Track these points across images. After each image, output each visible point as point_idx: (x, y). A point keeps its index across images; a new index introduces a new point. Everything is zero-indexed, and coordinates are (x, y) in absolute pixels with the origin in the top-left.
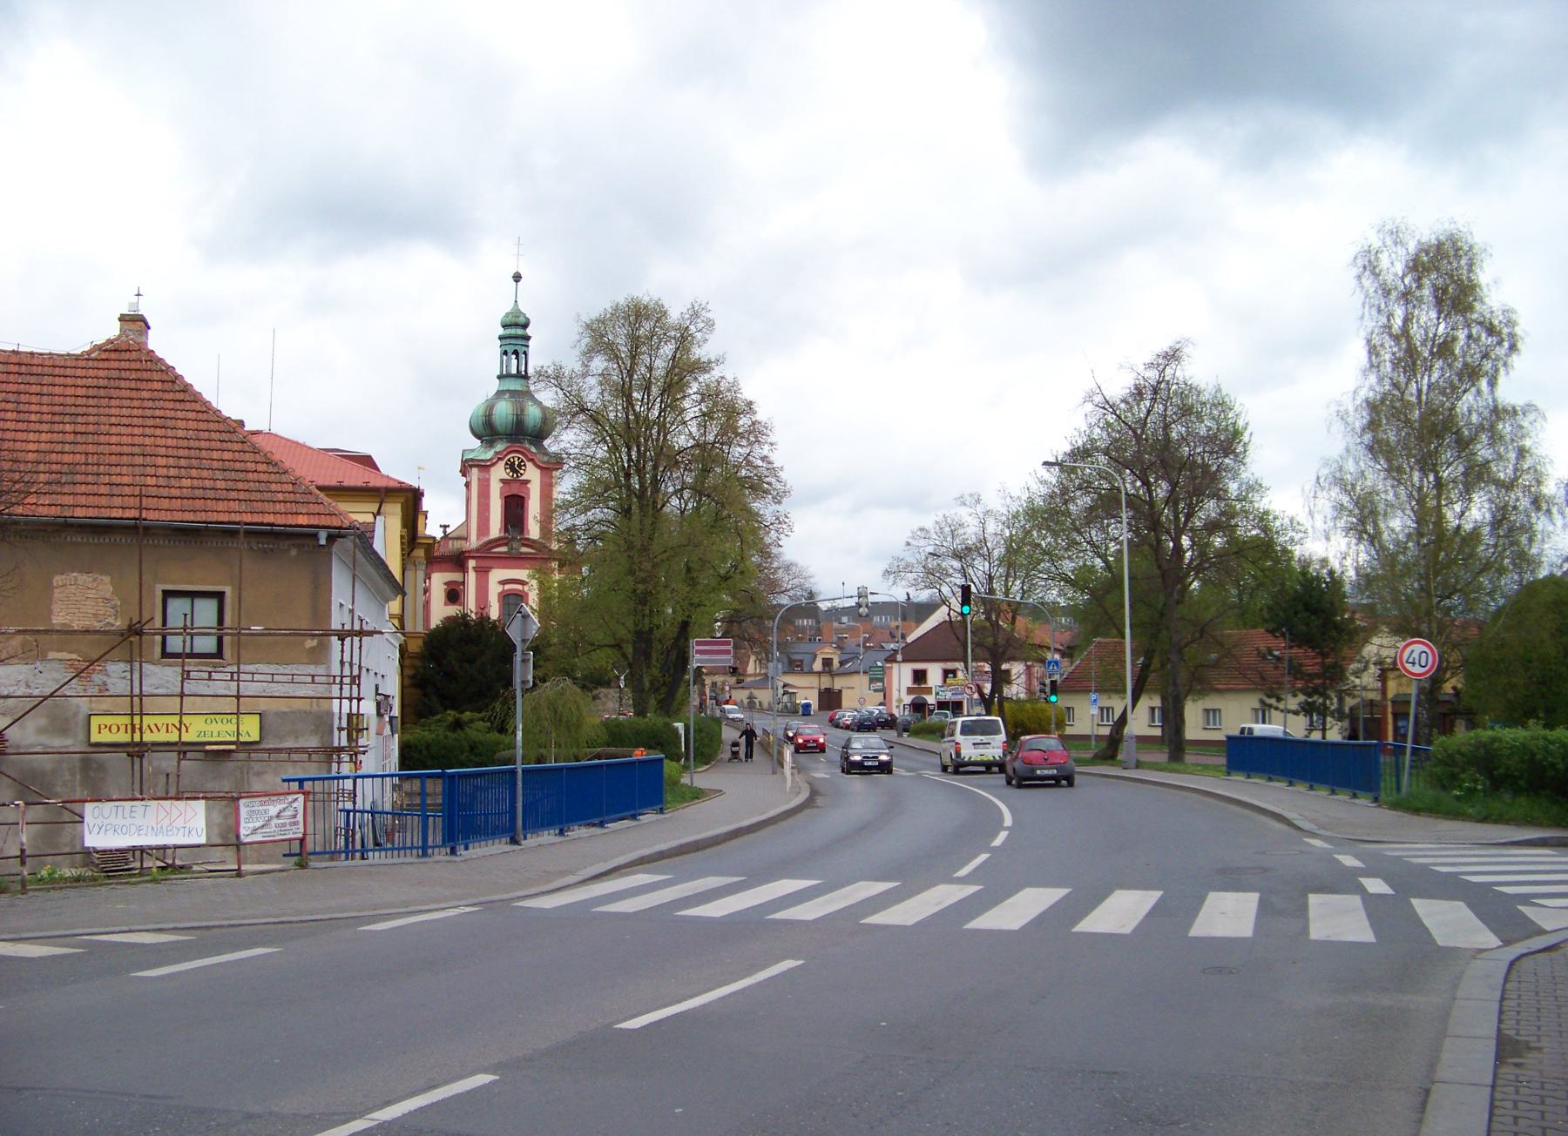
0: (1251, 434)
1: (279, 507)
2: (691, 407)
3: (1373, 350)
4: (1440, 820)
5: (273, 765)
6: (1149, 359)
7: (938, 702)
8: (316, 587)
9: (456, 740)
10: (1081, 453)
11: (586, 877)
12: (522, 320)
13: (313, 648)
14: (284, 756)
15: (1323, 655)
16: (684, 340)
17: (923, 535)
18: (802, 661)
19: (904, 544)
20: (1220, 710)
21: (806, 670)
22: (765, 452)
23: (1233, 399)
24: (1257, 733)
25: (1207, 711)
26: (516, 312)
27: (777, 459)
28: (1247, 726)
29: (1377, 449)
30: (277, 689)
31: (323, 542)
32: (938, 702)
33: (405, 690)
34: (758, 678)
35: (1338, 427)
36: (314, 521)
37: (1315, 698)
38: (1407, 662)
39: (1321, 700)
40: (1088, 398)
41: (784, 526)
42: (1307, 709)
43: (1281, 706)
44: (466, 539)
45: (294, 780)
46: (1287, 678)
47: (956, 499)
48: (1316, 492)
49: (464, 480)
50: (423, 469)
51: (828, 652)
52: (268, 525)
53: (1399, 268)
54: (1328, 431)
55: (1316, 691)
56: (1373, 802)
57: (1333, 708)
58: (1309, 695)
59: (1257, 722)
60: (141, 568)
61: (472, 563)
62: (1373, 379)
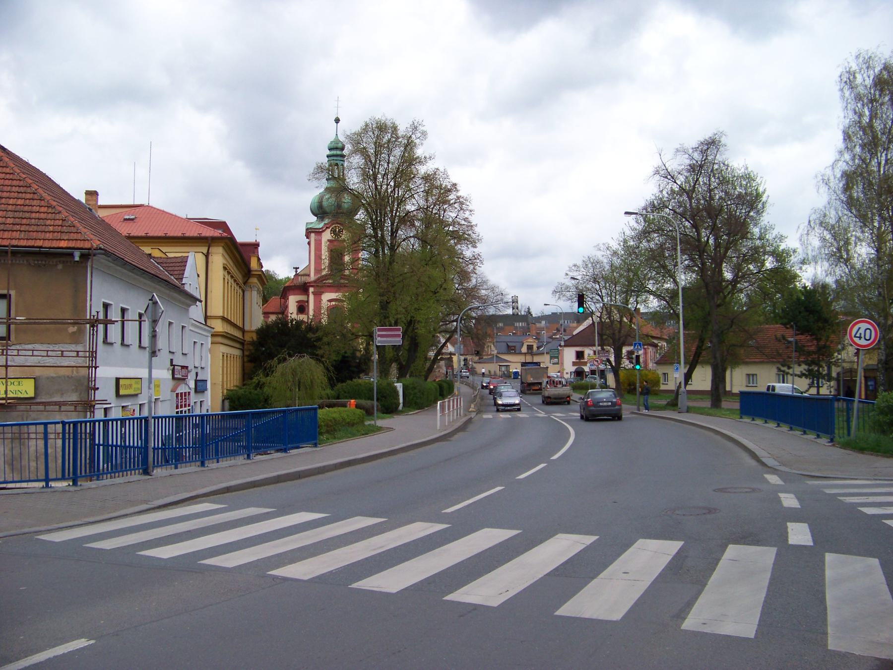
0: (768, 196)
1: (48, 236)
2: (418, 186)
3: (847, 137)
4: (879, 458)
5: (45, 413)
6: (695, 145)
7: (591, 371)
8: (76, 291)
9: (257, 394)
10: (656, 206)
11: (155, 506)
12: (340, 145)
13: (74, 333)
14: (41, 408)
15: (818, 340)
16: (409, 145)
17: (576, 269)
18: (515, 347)
19: (564, 274)
20: (756, 375)
21: (517, 352)
22: (466, 216)
23: (755, 174)
24: (777, 391)
25: (748, 375)
26: (337, 141)
27: (474, 220)
28: (771, 384)
29: (851, 203)
30: (50, 361)
31: (77, 258)
32: (591, 371)
33: (246, 364)
34: (489, 357)
35: (824, 189)
36: (72, 244)
37: (813, 367)
38: (855, 337)
39: (816, 368)
40: (657, 172)
41: (478, 261)
42: (809, 374)
43: (791, 371)
44: (309, 275)
45: (58, 423)
46: (794, 355)
47: (594, 247)
48: (808, 231)
49: (308, 240)
50: (258, 229)
51: (530, 341)
52: (37, 247)
53: (869, 82)
54: (818, 192)
55: (813, 362)
56: (829, 442)
57: (824, 373)
58: (809, 365)
59: (779, 382)
60: (9, 280)
61: (311, 290)
62: (847, 157)
